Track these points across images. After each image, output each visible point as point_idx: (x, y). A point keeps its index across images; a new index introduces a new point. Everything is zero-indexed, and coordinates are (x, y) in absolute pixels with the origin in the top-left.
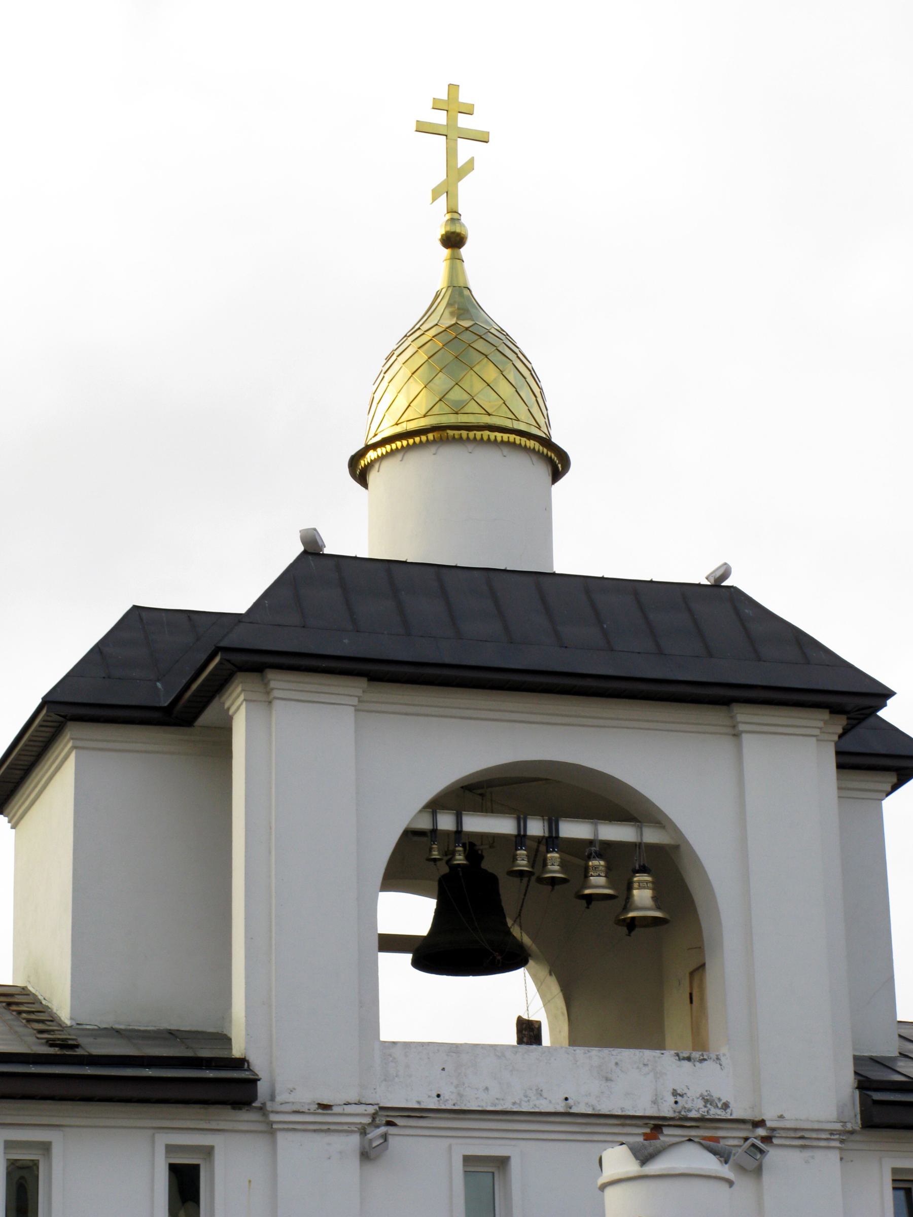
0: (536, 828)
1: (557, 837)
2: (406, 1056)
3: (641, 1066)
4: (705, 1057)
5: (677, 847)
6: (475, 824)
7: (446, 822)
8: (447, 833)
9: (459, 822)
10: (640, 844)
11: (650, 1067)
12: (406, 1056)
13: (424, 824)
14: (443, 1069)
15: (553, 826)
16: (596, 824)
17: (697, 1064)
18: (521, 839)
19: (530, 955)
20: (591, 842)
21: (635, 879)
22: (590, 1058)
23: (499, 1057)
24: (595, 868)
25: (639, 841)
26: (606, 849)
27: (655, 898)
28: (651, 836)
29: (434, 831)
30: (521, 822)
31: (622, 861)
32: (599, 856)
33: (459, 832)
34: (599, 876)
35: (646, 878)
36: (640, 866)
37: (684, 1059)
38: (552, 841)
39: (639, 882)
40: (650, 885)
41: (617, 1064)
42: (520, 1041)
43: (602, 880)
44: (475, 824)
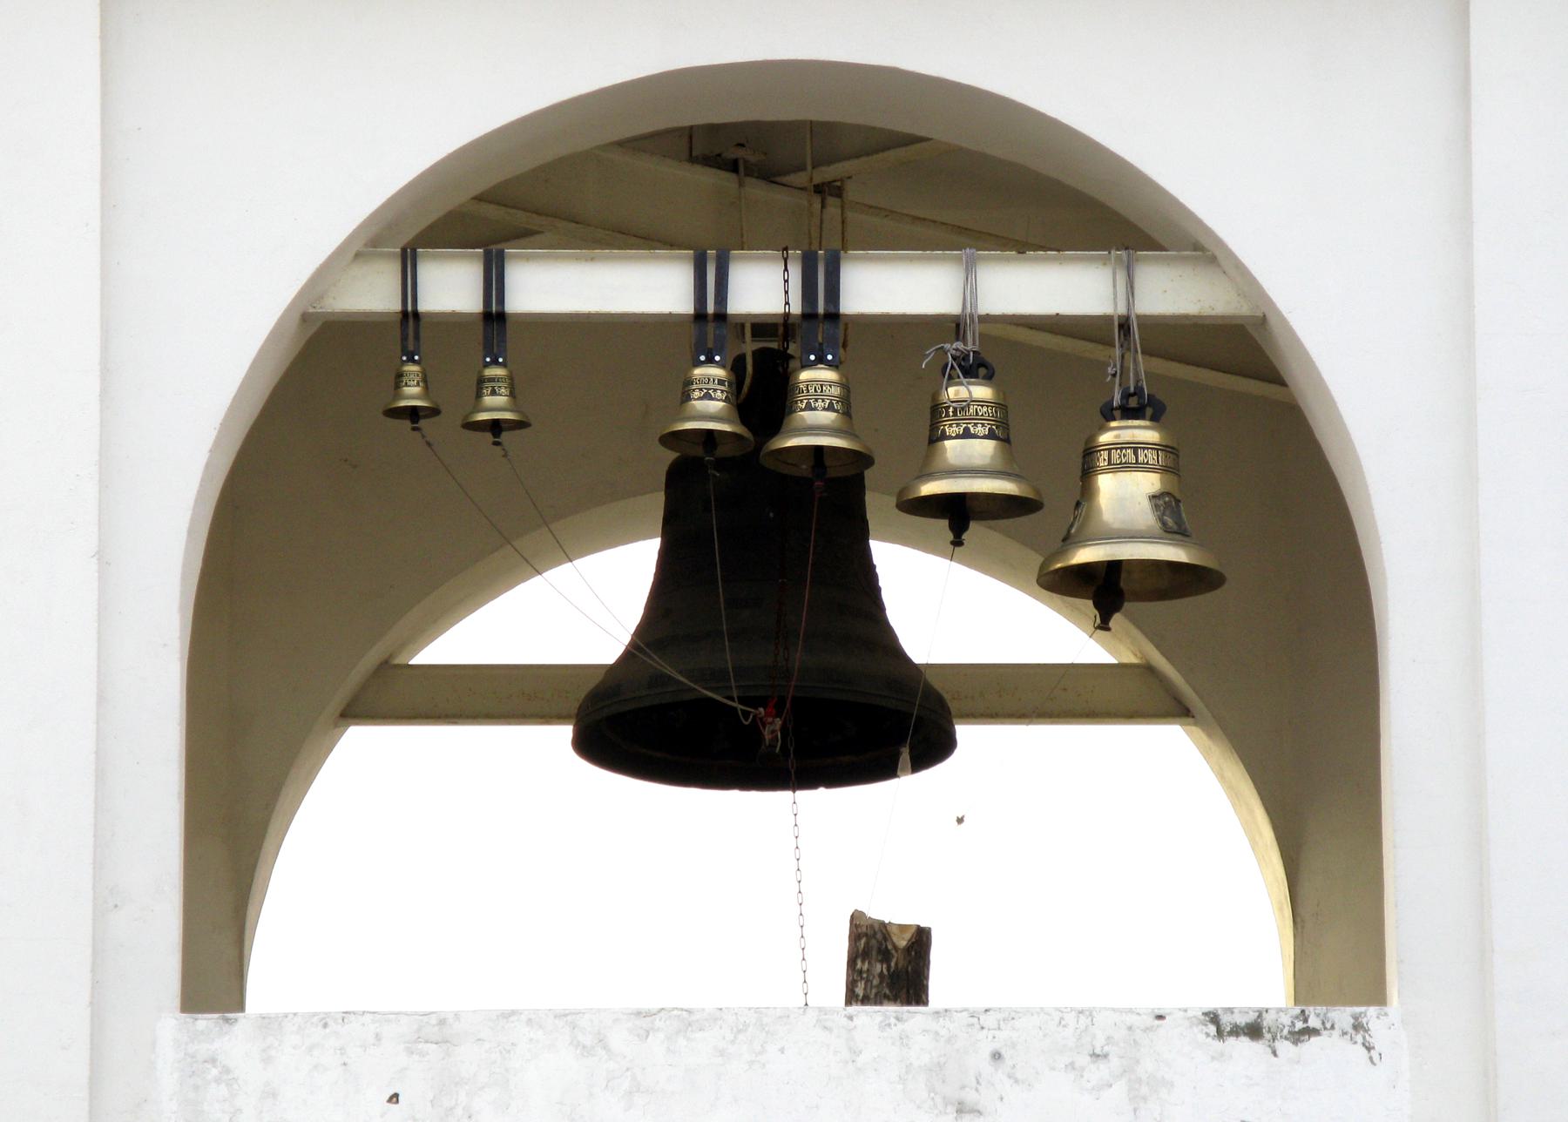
0: (761, 289)
1: (833, 316)
2: (267, 1060)
3: (1083, 1060)
4: (1314, 1022)
5: (1263, 320)
6: (547, 286)
7: (450, 287)
8: (451, 323)
9: (494, 283)
10: (1124, 325)
11: (1115, 1061)
12: (267, 1060)
13: (374, 293)
14: (394, 1098)
15: (820, 277)
16: (970, 269)
17: (1284, 1046)
18: (709, 325)
19: (953, 706)
20: (954, 326)
21: (1105, 438)
22: (903, 1039)
23: (586, 1051)
24: (963, 406)
25: (1122, 310)
26: (971, 345)
27: (1163, 502)
28: (1167, 292)
29: (410, 317)
30: (711, 272)
31: (1060, 383)
32: (973, 368)
33: (494, 318)
34: (967, 435)
35: (1143, 433)
36: (1126, 395)
37: (1236, 1031)
38: (820, 325)
39: (1120, 446)
40: (1151, 457)
41: (997, 1056)
42: (851, 998)
43: (982, 450)
44: (547, 286)
